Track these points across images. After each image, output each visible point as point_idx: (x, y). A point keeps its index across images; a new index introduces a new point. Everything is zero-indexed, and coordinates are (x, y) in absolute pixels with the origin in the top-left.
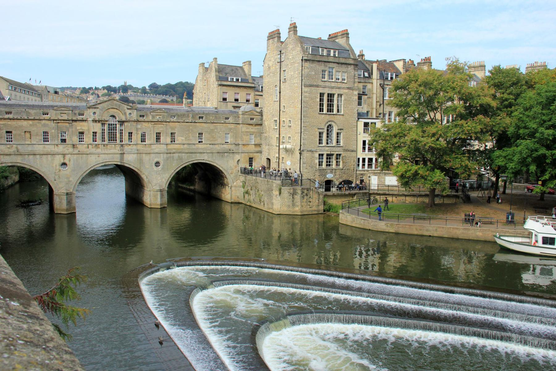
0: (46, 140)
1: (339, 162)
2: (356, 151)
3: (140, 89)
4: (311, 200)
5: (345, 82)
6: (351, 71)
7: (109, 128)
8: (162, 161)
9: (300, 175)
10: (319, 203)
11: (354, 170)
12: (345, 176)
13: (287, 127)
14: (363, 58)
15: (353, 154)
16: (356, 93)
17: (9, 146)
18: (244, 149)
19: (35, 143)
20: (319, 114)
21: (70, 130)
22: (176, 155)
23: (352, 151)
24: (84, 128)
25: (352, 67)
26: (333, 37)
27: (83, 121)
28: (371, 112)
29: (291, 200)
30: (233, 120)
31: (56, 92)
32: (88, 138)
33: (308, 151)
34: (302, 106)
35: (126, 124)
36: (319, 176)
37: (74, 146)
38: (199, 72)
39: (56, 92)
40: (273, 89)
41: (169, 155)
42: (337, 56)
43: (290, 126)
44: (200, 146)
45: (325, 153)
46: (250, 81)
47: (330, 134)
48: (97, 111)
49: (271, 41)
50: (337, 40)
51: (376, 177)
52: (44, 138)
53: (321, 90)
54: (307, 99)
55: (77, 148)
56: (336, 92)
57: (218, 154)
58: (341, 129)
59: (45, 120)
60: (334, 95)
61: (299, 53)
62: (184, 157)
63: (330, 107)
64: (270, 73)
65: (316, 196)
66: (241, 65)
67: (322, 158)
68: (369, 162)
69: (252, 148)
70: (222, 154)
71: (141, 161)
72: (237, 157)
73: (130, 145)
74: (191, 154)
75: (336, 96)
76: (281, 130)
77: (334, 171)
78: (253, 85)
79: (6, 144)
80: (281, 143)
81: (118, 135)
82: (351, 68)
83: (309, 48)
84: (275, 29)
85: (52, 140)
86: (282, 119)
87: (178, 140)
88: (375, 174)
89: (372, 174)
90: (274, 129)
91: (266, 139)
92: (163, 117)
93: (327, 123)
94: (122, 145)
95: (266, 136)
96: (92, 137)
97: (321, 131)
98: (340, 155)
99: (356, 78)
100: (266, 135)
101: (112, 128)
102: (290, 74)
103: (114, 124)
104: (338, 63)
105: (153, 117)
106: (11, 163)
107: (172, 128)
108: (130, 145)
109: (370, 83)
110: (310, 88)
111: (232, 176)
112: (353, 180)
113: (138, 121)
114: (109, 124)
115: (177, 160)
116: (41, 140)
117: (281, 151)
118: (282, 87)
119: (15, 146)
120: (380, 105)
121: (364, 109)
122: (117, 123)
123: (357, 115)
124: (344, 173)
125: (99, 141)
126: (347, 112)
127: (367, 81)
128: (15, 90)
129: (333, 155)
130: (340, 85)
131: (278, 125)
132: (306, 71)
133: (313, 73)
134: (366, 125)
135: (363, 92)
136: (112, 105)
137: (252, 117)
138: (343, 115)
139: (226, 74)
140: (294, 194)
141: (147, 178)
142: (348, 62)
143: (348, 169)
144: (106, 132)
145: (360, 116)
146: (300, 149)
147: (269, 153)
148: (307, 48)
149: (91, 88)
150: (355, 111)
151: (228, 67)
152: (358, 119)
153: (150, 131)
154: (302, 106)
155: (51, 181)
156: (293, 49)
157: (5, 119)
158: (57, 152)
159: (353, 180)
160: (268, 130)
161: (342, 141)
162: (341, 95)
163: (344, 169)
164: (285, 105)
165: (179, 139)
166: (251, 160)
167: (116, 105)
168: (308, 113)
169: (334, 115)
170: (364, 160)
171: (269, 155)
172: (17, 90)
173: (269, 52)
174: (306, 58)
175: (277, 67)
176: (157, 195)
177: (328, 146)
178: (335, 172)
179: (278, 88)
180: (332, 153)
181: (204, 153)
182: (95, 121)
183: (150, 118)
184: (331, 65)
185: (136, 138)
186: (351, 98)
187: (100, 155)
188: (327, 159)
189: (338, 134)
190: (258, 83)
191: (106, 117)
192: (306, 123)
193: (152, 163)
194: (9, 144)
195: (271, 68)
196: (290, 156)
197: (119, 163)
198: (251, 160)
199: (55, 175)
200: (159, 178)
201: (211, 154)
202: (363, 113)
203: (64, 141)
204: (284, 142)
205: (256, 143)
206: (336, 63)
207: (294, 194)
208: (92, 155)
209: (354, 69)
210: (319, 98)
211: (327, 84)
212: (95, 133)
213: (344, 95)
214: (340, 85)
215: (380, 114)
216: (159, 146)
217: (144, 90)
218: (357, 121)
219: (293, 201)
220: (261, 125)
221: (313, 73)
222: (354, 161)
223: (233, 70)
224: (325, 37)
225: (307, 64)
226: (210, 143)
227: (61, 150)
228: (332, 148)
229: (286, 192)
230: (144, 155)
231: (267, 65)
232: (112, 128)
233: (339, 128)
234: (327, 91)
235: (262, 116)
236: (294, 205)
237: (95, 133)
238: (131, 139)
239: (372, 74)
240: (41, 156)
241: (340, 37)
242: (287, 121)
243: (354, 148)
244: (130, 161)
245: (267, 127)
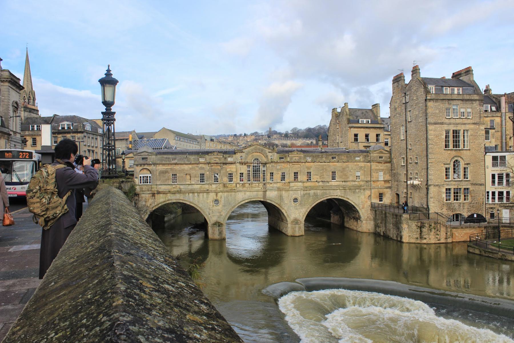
0: (202, 180)
1: (467, 196)
2: (484, 185)
3: (283, 134)
4: (438, 233)
5: (471, 117)
6: (476, 107)
7: (253, 169)
8: (300, 198)
9: (428, 209)
10: (447, 236)
11: (483, 203)
12: (474, 209)
13: (413, 164)
14: (490, 93)
15: (482, 188)
16: (483, 127)
17: (174, 186)
18: (374, 186)
19: (193, 183)
20: (445, 150)
21: (222, 172)
22: (312, 192)
23: (481, 185)
24: (232, 170)
25: (478, 102)
26: (456, 76)
27: (232, 164)
28: (500, 145)
29: (419, 232)
30: (364, 159)
31: (212, 140)
32: (236, 179)
33: (434, 186)
34: (427, 144)
35: (267, 165)
36: (447, 209)
37: (225, 186)
38: (332, 116)
39: (212, 140)
40: (399, 129)
41: (306, 192)
42: (461, 93)
43: (417, 163)
44: (334, 183)
45: (452, 187)
46: (379, 122)
47: (457, 168)
48: (243, 155)
49: (396, 84)
50: (461, 78)
51: (508, 211)
52: (201, 179)
53: (446, 127)
54: (433, 136)
55: (227, 187)
56: (461, 128)
57: (350, 190)
58: (468, 164)
59: (201, 164)
60: (459, 130)
61: (423, 93)
62: (319, 194)
63: (456, 143)
64: (397, 114)
65: (443, 229)
66: (371, 108)
67: (450, 193)
68: (499, 195)
69: (381, 184)
70: (353, 190)
71: (281, 197)
72: (368, 193)
73: (271, 183)
74: (325, 191)
75: (461, 133)
76: (409, 166)
77: (462, 205)
78: (382, 126)
79: (172, 185)
80: (409, 179)
81: (261, 175)
82: (476, 104)
83: (432, 88)
84: (399, 73)
85: (207, 181)
86: (409, 157)
87: (313, 179)
88: (506, 207)
89: (503, 208)
90: (402, 166)
91: (395, 176)
92: (300, 158)
93: (453, 158)
94: (265, 184)
95: (395, 173)
96: (239, 177)
97: (447, 166)
98: (468, 189)
99: (482, 113)
100: (395, 172)
101: (256, 171)
102: (414, 113)
103: (257, 166)
104: (462, 100)
105: (291, 159)
106: (176, 199)
107: (308, 168)
108: (271, 183)
109: (498, 116)
110: (435, 126)
111: (363, 211)
112: (483, 213)
113: (277, 162)
114: (253, 166)
115: (313, 196)
116: (198, 181)
117: (409, 187)
118: (408, 126)
119: (178, 186)
120: (510, 138)
121: (492, 142)
122: (260, 165)
123: (484, 150)
124: (473, 207)
125: (245, 181)
126: (474, 146)
127: (494, 115)
128: (180, 139)
129: (460, 189)
130: (466, 121)
131: (405, 162)
132: (429, 111)
133: (437, 111)
134: (495, 158)
135: (491, 126)
136: (256, 150)
137: (381, 155)
138: (469, 150)
139: (357, 117)
140: (421, 227)
141: (286, 212)
142: (472, 98)
143: (476, 203)
144: (251, 173)
145: (487, 150)
146: (427, 184)
147: (398, 189)
148: (430, 88)
149: (241, 135)
150: (483, 145)
151: (359, 111)
152: (486, 153)
153: (289, 171)
154: (427, 144)
155: (206, 215)
156: (416, 91)
157: (171, 164)
158: (211, 191)
159: (483, 213)
160: (396, 167)
161: (469, 176)
162: (467, 130)
163: (472, 202)
164: (412, 143)
165: (314, 178)
166: (381, 196)
167: (259, 149)
168: (434, 150)
169: (460, 150)
170: (493, 193)
171: (397, 190)
172: (181, 140)
173: (394, 94)
174: (428, 98)
175: (403, 108)
176: (295, 227)
177: (455, 181)
178: (463, 206)
179: (404, 128)
180: (459, 187)
181: (337, 190)
182: (241, 163)
183: (289, 159)
184: (455, 102)
185: (277, 177)
186: (477, 133)
187: (246, 193)
188: (454, 193)
189: (465, 168)
190: (387, 123)
191: (250, 159)
192: (432, 159)
193: (291, 199)
194: (174, 184)
195: (397, 109)
196: (418, 191)
197: (262, 200)
198: (381, 196)
199: (210, 210)
200: (297, 213)
201: (344, 190)
202: (491, 147)
203: (216, 180)
204: (411, 178)
205: (386, 179)
206: (460, 100)
207: (421, 227)
208: (239, 193)
209: (480, 105)
210: (445, 135)
211: (452, 121)
212: (242, 174)
213: (470, 130)
214: (466, 121)
215: (510, 147)
216: (296, 183)
217: (286, 136)
218: (485, 155)
219: (420, 234)
220: (390, 162)
221: (437, 111)
222: (483, 195)
223: (363, 113)
224: (449, 76)
225: (430, 104)
226: (343, 180)
227: (214, 189)
228: (459, 183)
229: (414, 225)
230: (284, 192)
231: (393, 107)
232: (256, 171)
233: (465, 163)
234: (452, 128)
235: (391, 154)
236: (421, 238)
237: (242, 174)
238: (273, 178)
239: (500, 108)
240: (199, 194)
241: (464, 74)
242: (414, 158)
243: (483, 181)
244: (272, 196)
245: (396, 165)
